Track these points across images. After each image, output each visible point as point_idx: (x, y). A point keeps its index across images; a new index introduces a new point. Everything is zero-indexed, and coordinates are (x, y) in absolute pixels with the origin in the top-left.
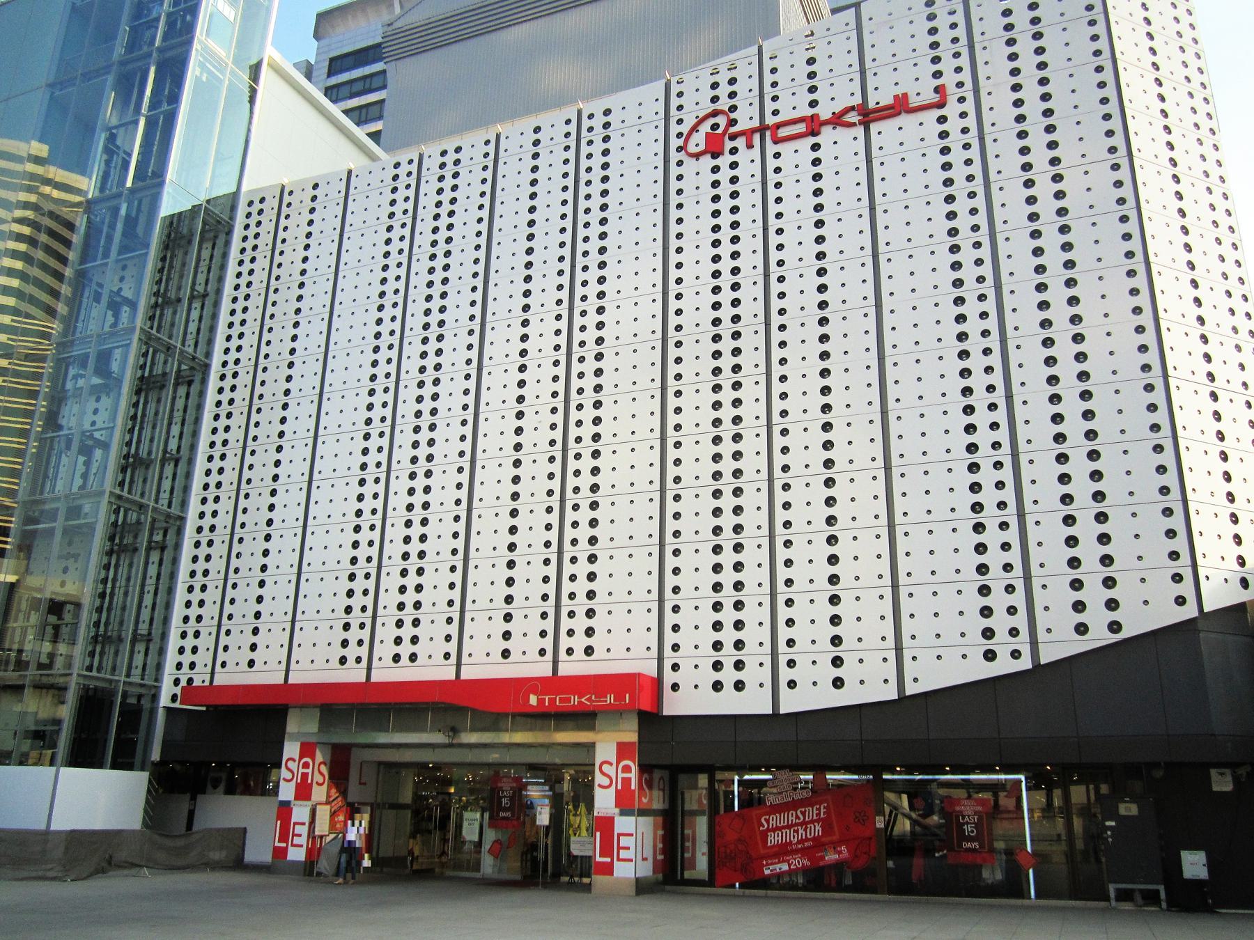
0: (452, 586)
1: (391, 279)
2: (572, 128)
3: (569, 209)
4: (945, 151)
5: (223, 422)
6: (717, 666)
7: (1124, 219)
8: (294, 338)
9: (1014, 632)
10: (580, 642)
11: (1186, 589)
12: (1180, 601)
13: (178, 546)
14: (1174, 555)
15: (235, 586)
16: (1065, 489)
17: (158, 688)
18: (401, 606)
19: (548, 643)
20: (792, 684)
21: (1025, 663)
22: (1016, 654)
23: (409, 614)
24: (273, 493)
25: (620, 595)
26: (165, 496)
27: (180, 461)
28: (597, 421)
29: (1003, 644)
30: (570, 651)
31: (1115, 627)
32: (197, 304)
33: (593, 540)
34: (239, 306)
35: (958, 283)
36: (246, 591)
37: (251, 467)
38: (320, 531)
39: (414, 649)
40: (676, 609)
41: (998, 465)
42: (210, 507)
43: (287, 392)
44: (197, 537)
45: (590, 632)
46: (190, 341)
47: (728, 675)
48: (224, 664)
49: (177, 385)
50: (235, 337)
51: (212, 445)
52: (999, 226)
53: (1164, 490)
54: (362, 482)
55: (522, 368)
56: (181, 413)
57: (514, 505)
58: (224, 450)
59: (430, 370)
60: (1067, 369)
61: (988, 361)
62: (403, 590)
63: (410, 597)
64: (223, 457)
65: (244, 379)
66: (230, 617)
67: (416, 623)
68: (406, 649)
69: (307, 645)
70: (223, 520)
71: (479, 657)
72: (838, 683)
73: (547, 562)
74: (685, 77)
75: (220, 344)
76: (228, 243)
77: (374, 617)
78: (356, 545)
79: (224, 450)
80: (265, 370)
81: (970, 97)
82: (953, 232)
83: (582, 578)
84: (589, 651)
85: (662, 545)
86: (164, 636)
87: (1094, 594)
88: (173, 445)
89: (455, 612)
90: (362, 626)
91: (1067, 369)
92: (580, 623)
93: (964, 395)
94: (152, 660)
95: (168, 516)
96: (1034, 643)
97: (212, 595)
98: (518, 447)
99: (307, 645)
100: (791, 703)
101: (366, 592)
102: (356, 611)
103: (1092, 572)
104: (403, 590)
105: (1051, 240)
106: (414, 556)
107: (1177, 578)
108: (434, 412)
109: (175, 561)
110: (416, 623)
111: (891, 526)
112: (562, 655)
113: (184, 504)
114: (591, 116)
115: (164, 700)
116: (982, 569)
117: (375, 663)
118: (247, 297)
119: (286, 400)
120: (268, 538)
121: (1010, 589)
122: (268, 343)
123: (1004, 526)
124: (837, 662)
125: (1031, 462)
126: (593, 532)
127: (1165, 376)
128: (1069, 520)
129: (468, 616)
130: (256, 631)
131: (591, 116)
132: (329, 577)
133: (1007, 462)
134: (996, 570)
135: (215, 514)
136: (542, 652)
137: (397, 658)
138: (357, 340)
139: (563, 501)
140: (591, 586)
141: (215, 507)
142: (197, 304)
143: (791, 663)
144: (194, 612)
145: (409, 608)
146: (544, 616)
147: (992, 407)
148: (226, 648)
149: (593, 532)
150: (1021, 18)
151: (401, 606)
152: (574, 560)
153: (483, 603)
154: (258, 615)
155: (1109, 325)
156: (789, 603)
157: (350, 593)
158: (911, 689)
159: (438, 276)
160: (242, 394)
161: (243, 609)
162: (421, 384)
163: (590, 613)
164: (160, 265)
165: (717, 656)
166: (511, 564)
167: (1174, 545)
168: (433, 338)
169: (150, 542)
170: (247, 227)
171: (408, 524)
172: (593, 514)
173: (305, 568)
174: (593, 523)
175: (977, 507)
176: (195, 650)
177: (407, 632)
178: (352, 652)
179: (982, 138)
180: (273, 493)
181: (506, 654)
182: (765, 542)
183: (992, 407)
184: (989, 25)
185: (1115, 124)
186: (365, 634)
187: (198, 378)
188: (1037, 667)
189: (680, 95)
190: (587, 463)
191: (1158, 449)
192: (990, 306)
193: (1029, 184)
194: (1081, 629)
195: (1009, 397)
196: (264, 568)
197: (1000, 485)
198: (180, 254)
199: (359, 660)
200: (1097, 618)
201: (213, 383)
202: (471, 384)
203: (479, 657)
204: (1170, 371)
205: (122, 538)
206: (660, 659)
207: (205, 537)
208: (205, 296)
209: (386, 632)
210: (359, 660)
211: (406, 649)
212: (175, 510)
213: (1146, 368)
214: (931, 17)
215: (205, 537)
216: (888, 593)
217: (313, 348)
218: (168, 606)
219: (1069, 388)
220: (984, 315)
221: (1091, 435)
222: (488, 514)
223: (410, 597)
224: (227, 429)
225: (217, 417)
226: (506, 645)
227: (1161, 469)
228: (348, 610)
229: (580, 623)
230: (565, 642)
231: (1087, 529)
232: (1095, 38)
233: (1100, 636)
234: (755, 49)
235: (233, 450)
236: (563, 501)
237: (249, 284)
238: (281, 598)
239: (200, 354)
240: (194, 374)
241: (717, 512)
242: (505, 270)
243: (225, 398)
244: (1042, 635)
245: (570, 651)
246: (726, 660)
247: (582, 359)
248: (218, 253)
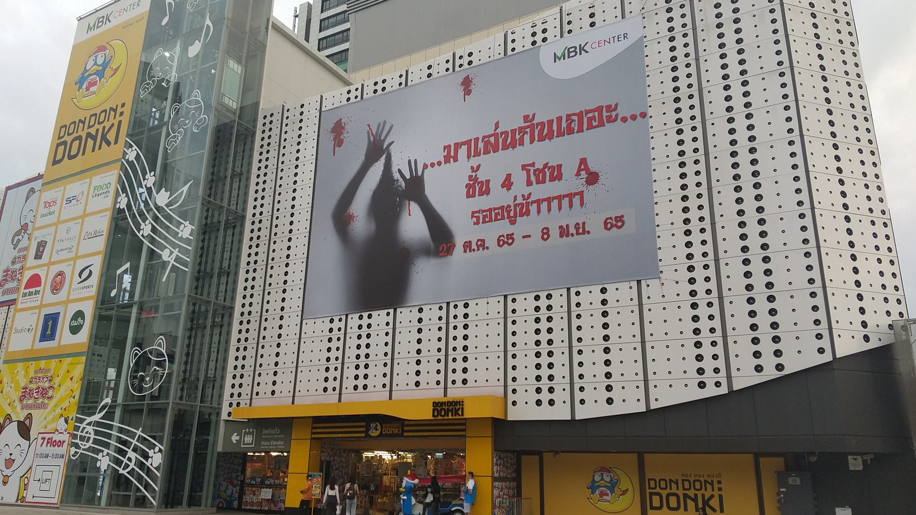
4: (685, 198)
5: (260, 202)
6: (538, 355)
7: (787, 108)
8: (296, 175)
9: (716, 370)
10: (459, 377)
11: (825, 343)
12: (821, 351)
13: (230, 324)
14: (809, 268)
15: (260, 375)
16: (747, 268)
17: (220, 409)
18: (358, 357)
19: (441, 377)
20: (582, 402)
21: (723, 390)
22: (718, 384)
23: (362, 361)
24: (284, 291)
25: (482, 348)
26: (221, 295)
27: (229, 274)
28: (466, 337)
29: (709, 377)
30: (454, 382)
31: (779, 367)
32: (236, 180)
34: (263, 165)
35: (676, 89)
36: (269, 351)
37: (268, 302)
38: (309, 341)
39: (367, 351)
40: (514, 356)
41: (708, 292)
42: (251, 275)
43: (293, 207)
44: (244, 293)
45: (466, 337)
46: (233, 202)
47: (545, 396)
48: (257, 394)
49: (225, 229)
50: (256, 230)
51: (251, 239)
52: (708, 116)
53: (815, 308)
54: (330, 340)
56: (216, 345)
58: (261, 217)
60: (742, 135)
61: (711, 311)
63: (363, 351)
64: (255, 270)
65: (266, 224)
66: (264, 338)
67: (366, 366)
68: (361, 382)
69: (305, 381)
70: (256, 308)
71: (402, 386)
72: (610, 401)
73: (439, 361)
74: (516, 30)
75: (251, 203)
76: (253, 142)
77: (343, 364)
78: (326, 380)
79: (261, 217)
80: (272, 268)
81: (690, 33)
82: (671, 29)
84: (465, 382)
85: (505, 318)
86: (223, 378)
87: (768, 347)
88: (226, 264)
89: (388, 360)
90: (336, 369)
91: (738, 102)
92: (460, 332)
93: (685, 224)
94: (221, 356)
95: (224, 307)
96: (729, 377)
97: (250, 353)
99: (305, 381)
100: (582, 413)
101: (338, 349)
102: (333, 360)
103: (761, 293)
104: (359, 347)
105: (737, 91)
106: (363, 357)
107: (819, 336)
109: (229, 333)
111: (643, 342)
112: (450, 384)
113: (233, 299)
114: (461, 57)
115: (224, 416)
116: (693, 293)
117: (344, 390)
118: (269, 137)
119: (293, 211)
120: (282, 318)
121: (706, 267)
122: (286, 132)
123: (694, 129)
124: (607, 350)
125: (727, 264)
127: (813, 208)
128: (751, 301)
129: (396, 362)
130: (279, 345)
131: (461, 57)
132: (317, 340)
133: (712, 265)
134: (709, 372)
135: (257, 254)
136: (438, 383)
137: (356, 388)
139: (447, 323)
141: (254, 275)
142: (236, 180)
143: (579, 328)
144: (240, 363)
145: (365, 328)
146: (440, 329)
147: (703, 230)
148: (262, 356)
150: (727, 8)
151: (358, 357)
153: (404, 354)
154: (285, 282)
155: (777, 188)
156: (581, 364)
157: (329, 350)
158: (654, 405)
160: (265, 233)
161: (268, 361)
163: (465, 359)
164: (205, 214)
165: (538, 349)
167: (811, 274)
169: (214, 322)
170: (264, 132)
171: (359, 337)
173: (303, 335)
175: (701, 371)
176: (244, 358)
177: (364, 341)
178: (330, 384)
179: (697, 59)
180: (284, 291)
181: (417, 384)
182: (565, 316)
183: (714, 344)
184: (705, 15)
185: (802, 184)
186: (340, 344)
187: (238, 224)
188: (731, 392)
189: (513, 41)
191: (807, 255)
192: (692, 70)
193: (738, 189)
194: (759, 369)
195: (713, 224)
196: (280, 336)
197: (706, 267)
198: (220, 185)
199: (334, 389)
200: (769, 362)
201: (248, 226)
203: (402, 386)
204: (816, 205)
205: (198, 320)
206: (506, 386)
207: (249, 292)
208: (241, 174)
209: (350, 372)
210: (334, 389)
211: (361, 382)
212: (227, 303)
213: (800, 203)
214: (669, 10)
215: (249, 292)
216: (639, 346)
217: (300, 255)
218: (225, 360)
219: (739, 112)
220: (707, 279)
221: (765, 247)
223: (363, 351)
224: (267, 159)
225: (250, 247)
227: (804, 229)
229: (459, 365)
230: (451, 376)
231: (757, 267)
232: (778, 53)
233: (770, 373)
234: (559, 8)
235: (258, 291)
236: (447, 323)
237: (266, 167)
238: (293, 325)
239: (239, 210)
240: (236, 222)
241: (538, 366)
243: (260, 188)
244: (734, 372)
245: (454, 382)
246: (544, 387)
248: (247, 147)
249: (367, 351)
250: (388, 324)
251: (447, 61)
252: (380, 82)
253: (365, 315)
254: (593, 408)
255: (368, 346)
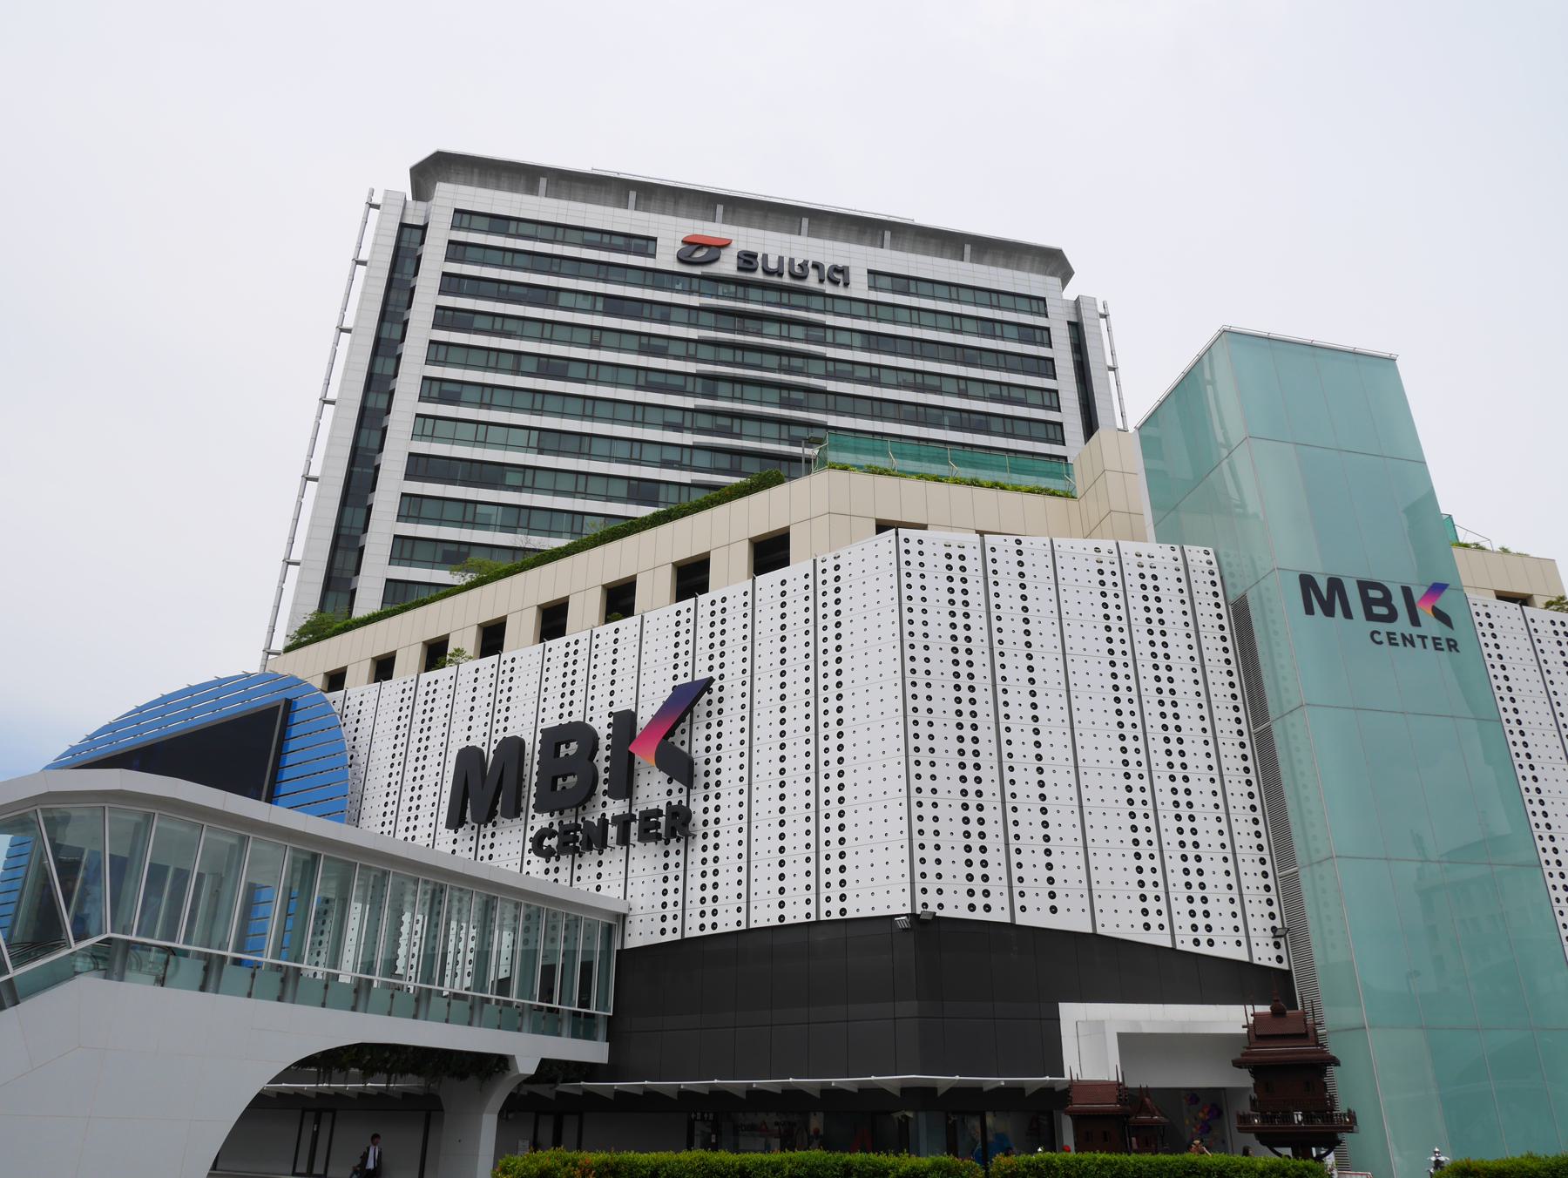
0: (740, 869)
1: (682, 654)
2: (810, 581)
3: (810, 615)
18: (703, 900)
21: (678, 936)
25: (864, 839)
28: (841, 827)
33: (841, 761)
39: (716, 879)
54: (665, 880)
55: (783, 639)
57: (782, 817)
59: (717, 655)
62: (703, 887)
83: (834, 788)
89: (742, 903)
98: (783, 709)
100: (1022, 919)
101: (677, 865)
108: (722, 643)
110: (715, 912)
126: (842, 862)
138: (661, 660)
140: (842, 834)
145: (718, 613)
149: (840, 754)
152: (828, 899)
153: (763, 814)
157: (665, 892)
159: (717, 639)
162: (711, 657)
163: (842, 855)
166: (782, 784)
168: (717, 655)
172: (840, 754)
174: (842, 869)
190: (835, 863)
202: (748, 654)
222: (763, 825)
224: (571, 703)
226: (782, 884)
228: (664, 905)
242: (765, 738)
247: (826, 725)
249: (716, 853)
250: (739, 896)
251: (806, 576)
252: (718, 601)
253: (708, 931)
254: (1035, 917)
255: (715, 886)
